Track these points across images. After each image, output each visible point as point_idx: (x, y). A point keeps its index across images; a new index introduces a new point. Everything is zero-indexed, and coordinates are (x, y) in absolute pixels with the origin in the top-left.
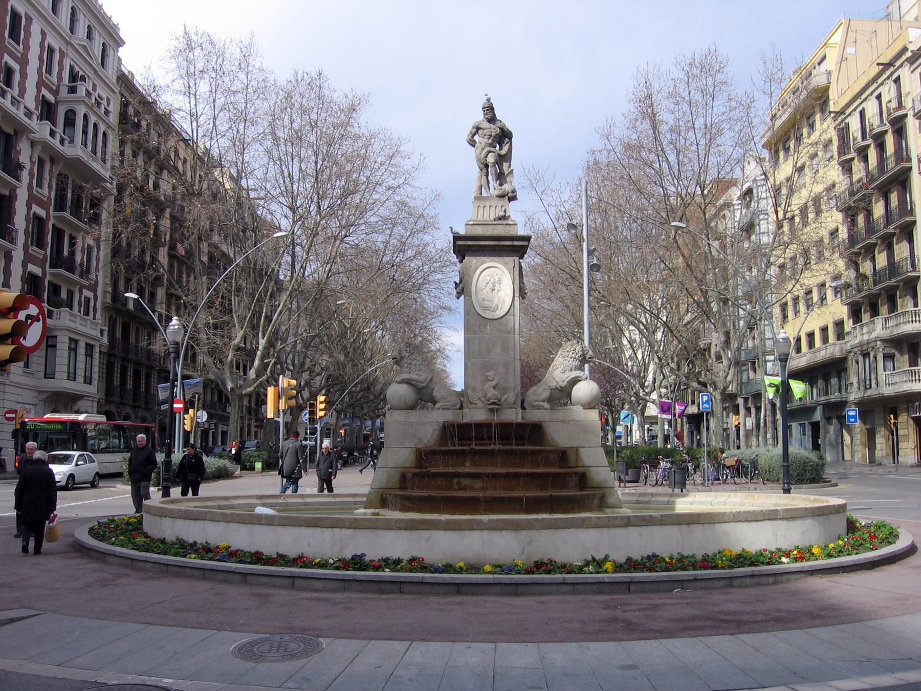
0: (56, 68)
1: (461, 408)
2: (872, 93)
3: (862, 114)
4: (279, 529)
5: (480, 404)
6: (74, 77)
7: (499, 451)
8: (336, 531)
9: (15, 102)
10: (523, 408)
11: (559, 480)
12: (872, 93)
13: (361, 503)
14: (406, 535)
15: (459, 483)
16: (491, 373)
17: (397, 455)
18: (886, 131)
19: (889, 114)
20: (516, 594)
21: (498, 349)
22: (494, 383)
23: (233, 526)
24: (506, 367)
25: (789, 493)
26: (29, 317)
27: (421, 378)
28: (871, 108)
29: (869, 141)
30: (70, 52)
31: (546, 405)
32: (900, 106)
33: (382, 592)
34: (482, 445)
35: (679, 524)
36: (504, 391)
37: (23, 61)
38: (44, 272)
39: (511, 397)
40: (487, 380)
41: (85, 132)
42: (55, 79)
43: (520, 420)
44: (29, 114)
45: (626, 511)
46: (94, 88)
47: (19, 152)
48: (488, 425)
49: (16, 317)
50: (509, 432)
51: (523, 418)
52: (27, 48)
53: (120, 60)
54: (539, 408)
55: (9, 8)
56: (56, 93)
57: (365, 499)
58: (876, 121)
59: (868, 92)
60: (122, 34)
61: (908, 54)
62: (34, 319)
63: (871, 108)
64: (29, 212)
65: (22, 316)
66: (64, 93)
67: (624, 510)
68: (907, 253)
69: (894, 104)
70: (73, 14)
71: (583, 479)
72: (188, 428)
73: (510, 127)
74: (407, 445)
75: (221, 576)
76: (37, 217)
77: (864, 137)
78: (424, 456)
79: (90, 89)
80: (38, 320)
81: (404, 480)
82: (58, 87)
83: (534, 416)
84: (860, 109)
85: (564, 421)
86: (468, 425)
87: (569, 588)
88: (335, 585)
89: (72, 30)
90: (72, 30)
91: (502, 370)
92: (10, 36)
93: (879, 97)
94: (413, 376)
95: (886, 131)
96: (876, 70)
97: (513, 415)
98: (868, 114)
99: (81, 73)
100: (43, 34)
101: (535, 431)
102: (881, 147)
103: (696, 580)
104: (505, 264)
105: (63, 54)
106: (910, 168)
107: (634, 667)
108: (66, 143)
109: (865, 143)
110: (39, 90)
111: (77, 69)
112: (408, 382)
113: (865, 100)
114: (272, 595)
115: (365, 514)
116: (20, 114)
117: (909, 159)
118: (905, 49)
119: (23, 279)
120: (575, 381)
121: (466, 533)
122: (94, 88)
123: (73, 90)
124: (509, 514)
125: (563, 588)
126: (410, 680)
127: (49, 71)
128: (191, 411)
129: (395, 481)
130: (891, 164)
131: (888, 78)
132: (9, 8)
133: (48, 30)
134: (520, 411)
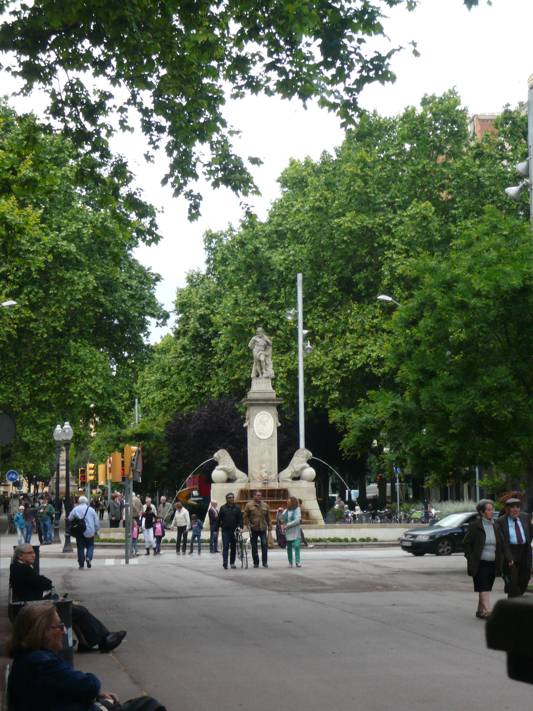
5: (259, 480)
16: (263, 465)
21: (267, 453)
24: (271, 462)
27: (229, 468)
36: (270, 473)
39: (274, 475)
40: (262, 468)
54: (286, 481)
83: (284, 486)
85: (298, 488)
91: (269, 464)
94: (226, 467)
97: (274, 485)
104: (270, 412)
112: (223, 469)
120: (303, 468)
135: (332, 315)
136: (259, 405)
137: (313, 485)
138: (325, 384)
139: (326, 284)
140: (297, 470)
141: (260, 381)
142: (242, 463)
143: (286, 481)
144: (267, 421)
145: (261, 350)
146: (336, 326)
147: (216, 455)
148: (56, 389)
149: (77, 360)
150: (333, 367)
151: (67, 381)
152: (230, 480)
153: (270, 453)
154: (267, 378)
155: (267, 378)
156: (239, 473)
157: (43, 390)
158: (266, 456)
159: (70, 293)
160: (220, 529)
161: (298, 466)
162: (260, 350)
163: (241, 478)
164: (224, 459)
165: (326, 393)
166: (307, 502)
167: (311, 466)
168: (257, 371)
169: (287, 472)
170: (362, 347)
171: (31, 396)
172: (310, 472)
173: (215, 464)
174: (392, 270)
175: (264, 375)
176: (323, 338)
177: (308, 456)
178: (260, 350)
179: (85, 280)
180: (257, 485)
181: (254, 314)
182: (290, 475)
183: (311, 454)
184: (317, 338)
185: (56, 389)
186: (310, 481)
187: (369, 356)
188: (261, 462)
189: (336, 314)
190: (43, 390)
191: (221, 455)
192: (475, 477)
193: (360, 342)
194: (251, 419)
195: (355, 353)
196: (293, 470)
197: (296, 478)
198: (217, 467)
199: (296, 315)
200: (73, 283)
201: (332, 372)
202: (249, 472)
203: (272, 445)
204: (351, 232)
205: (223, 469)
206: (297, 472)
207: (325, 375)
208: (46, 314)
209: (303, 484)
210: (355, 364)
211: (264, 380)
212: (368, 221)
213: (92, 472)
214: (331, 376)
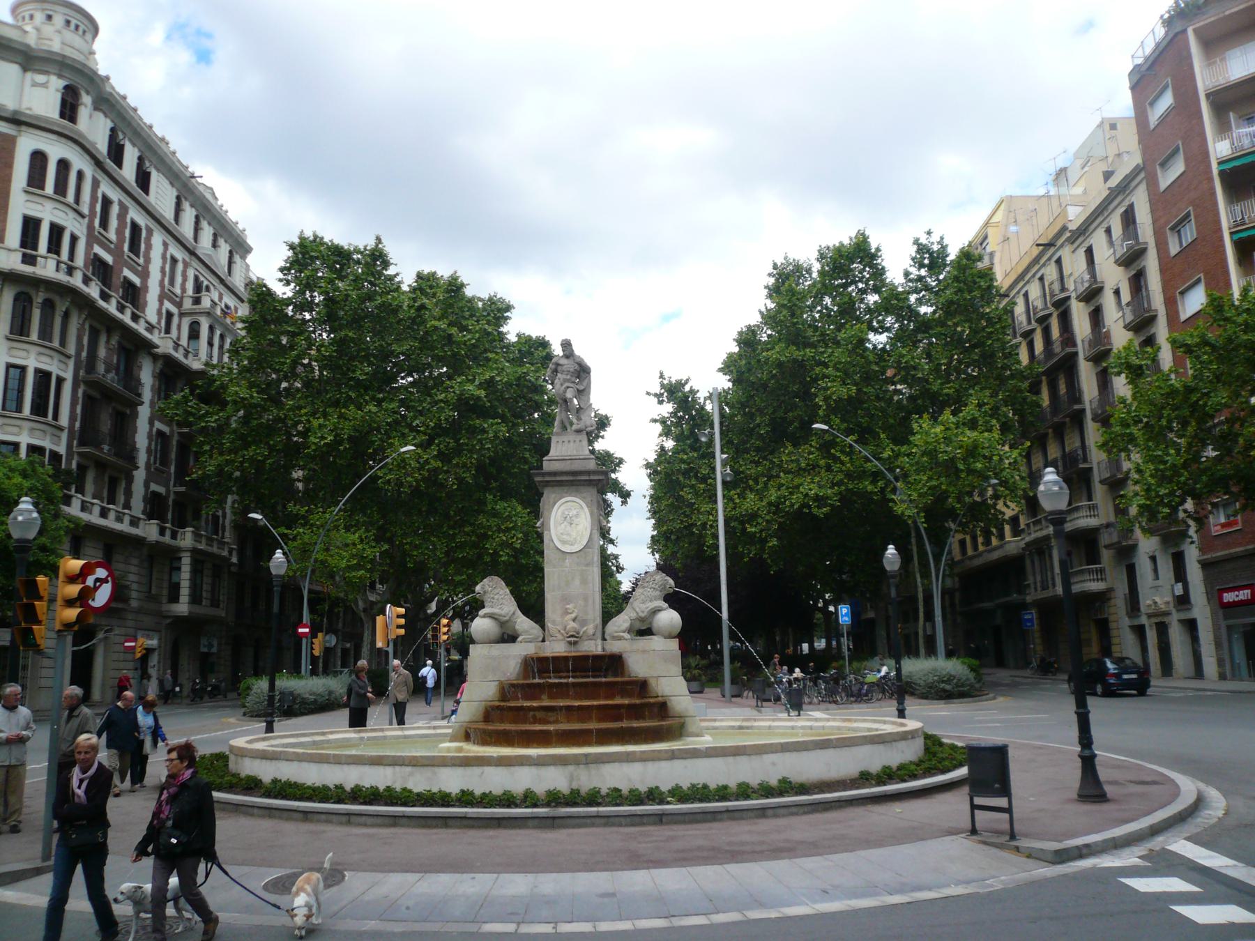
0: (179, 279)
1: (543, 641)
2: (1034, 276)
3: (1026, 295)
4: (346, 767)
5: (560, 637)
6: (198, 287)
7: (574, 684)
8: (397, 768)
9: (135, 318)
10: (604, 639)
11: (636, 712)
12: (1034, 276)
13: (445, 735)
14: (459, 771)
15: (534, 717)
17: (480, 689)
18: (1050, 315)
19: (1052, 295)
20: (553, 827)
21: (577, 582)
22: (573, 615)
23: (305, 765)
24: (586, 599)
25: (19, 831)
26: (97, 580)
27: (503, 613)
28: (1034, 291)
29: (1034, 324)
30: (195, 263)
31: (626, 635)
32: (1063, 289)
33: (429, 827)
34: (561, 677)
35: (725, 755)
36: (584, 623)
37: (145, 275)
38: (168, 491)
39: (590, 628)
40: (566, 612)
41: (210, 344)
42: (178, 290)
43: (599, 651)
44: (150, 328)
45: (706, 741)
46: (221, 299)
47: (140, 368)
48: (566, 658)
49: (84, 582)
50: (584, 664)
51: (604, 649)
52: (148, 260)
53: (248, 266)
54: (620, 638)
55: (128, 221)
56: (179, 305)
57: (450, 731)
58: (1039, 304)
59: (1029, 275)
60: (250, 241)
61: (1068, 234)
62: (105, 581)
63: (1034, 291)
64: (151, 430)
65: (90, 581)
66: (188, 304)
67: (707, 738)
68: (1078, 444)
69: (1056, 287)
70: (197, 222)
71: (662, 709)
72: (316, 653)
73: (589, 361)
74: (490, 678)
75: (285, 814)
76: (160, 433)
77: (1029, 322)
78: (507, 691)
79: (216, 300)
80: (107, 582)
81: (489, 714)
82: (182, 298)
83: (614, 647)
84: (1023, 292)
85: (644, 651)
86: (546, 659)
87: (603, 821)
88: (387, 821)
89: (196, 239)
90: (196, 239)
91: (581, 602)
92: (131, 250)
93: (1041, 279)
94: (496, 610)
95: (1050, 315)
96: (1036, 251)
97: (593, 647)
98: (1032, 297)
99: (206, 283)
100: (165, 245)
101: (614, 662)
102: (1047, 332)
103: (728, 811)
104: (583, 499)
105: (186, 265)
106: (1076, 354)
107: (613, 895)
108: (190, 356)
109: (1030, 327)
110: (161, 303)
111: (202, 279)
112: (491, 616)
113: (1028, 282)
114: (324, 831)
115: (448, 750)
116: (140, 328)
117: (1075, 345)
118: (1064, 229)
119: (145, 499)
120: (656, 611)
121: (516, 768)
122: (221, 299)
123: (197, 301)
124: (623, 744)
125: (598, 821)
126: (408, 908)
127: (172, 282)
128: (320, 635)
129: (480, 716)
130: (1057, 348)
131: (1049, 259)
132: (128, 221)
133: (170, 240)
134: (599, 642)
135: (765, 458)
136: (560, 484)
137: (674, 645)
138: (761, 531)
139: (758, 425)
140: (643, 615)
141: (565, 438)
142: (533, 607)
143: (620, 638)
144: (577, 516)
145: (568, 381)
146: (770, 469)
147: (478, 588)
148: (474, 545)
149: (495, 514)
150: (769, 512)
151: (485, 537)
152: (508, 637)
153: (584, 581)
154: (579, 431)
155: (579, 431)
156: (523, 623)
157: (462, 546)
158: (576, 587)
159: (480, 441)
160: (79, 867)
161: (643, 606)
162: (566, 381)
163: (526, 632)
164: (497, 597)
165: (763, 541)
166: (663, 680)
167: (671, 607)
168: (562, 422)
169: (621, 622)
170: (797, 487)
171: (447, 554)
172: (670, 618)
173: (476, 606)
174: (826, 399)
175: (574, 427)
176: (757, 483)
177: (663, 587)
178: (566, 381)
179: (495, 429)
180: (557, 648)
181: (682, 461)
182: (626, 625)
183: (671, 582)
184: (751, 482)
185: (474, 545)
186: (670, 637)
187: (807, 495)
188: (566, 599)
189: (770, 457)
190: (462, 546)
191: (487, 588)
192: (607, 698)
193: (797, 481)
194: (545, 513)
195: (791, 493)
196: (633, 615)
197: (644, 630)
198: (482, 612)
199: (712, 435)
200: (484, 431)
201: (768, 517)
202: (549, 624)
203: (587, 565)
204: (780, 365)
205: (491, 616)
206: (642, 620)
207: (760, 520)
208: (457, 465)
209: (656, 643)
210: (792, 505)
211: (572, 437)
212: (798, 354)
213: (445, 629)
214: (767, 521)
